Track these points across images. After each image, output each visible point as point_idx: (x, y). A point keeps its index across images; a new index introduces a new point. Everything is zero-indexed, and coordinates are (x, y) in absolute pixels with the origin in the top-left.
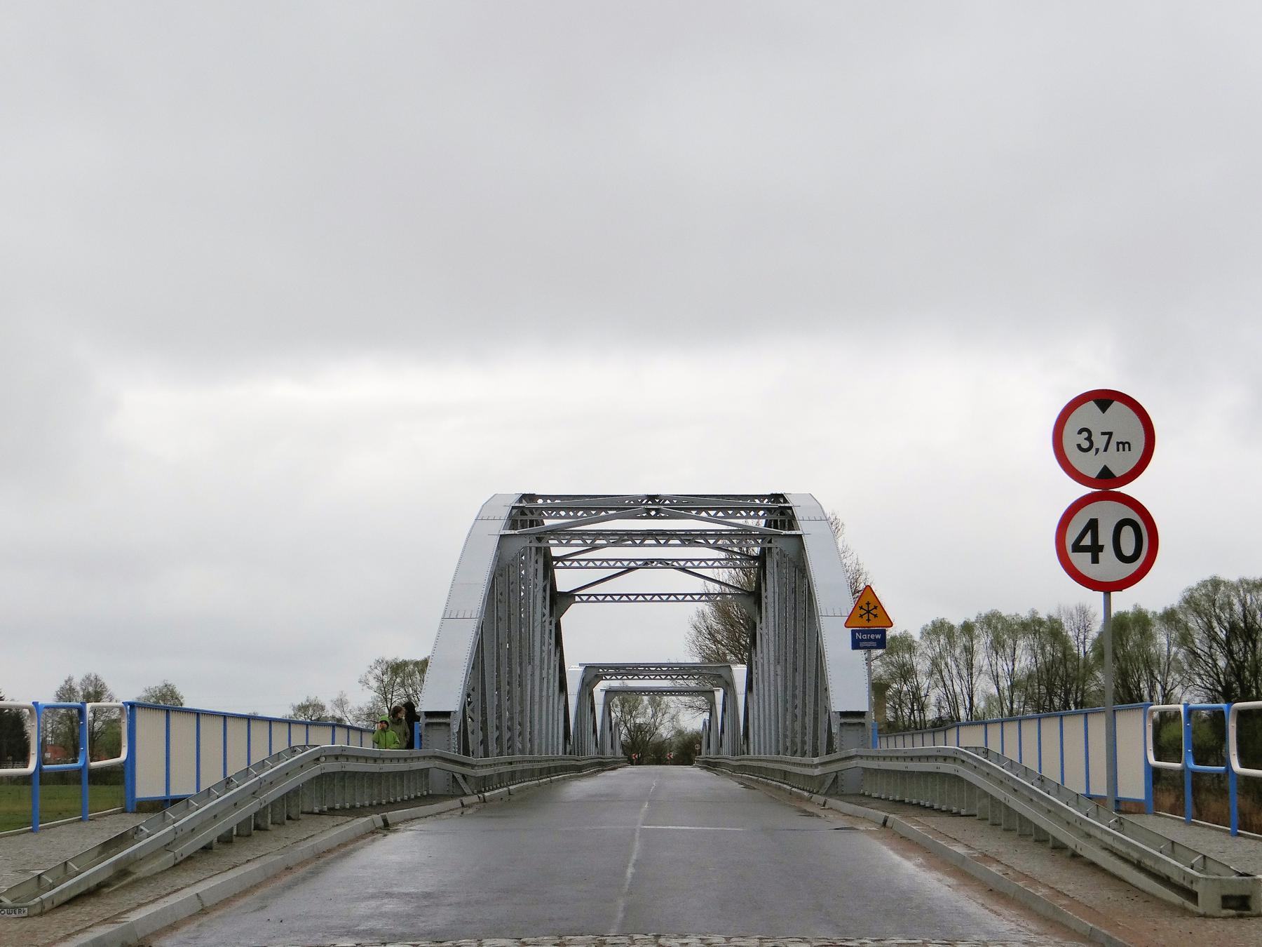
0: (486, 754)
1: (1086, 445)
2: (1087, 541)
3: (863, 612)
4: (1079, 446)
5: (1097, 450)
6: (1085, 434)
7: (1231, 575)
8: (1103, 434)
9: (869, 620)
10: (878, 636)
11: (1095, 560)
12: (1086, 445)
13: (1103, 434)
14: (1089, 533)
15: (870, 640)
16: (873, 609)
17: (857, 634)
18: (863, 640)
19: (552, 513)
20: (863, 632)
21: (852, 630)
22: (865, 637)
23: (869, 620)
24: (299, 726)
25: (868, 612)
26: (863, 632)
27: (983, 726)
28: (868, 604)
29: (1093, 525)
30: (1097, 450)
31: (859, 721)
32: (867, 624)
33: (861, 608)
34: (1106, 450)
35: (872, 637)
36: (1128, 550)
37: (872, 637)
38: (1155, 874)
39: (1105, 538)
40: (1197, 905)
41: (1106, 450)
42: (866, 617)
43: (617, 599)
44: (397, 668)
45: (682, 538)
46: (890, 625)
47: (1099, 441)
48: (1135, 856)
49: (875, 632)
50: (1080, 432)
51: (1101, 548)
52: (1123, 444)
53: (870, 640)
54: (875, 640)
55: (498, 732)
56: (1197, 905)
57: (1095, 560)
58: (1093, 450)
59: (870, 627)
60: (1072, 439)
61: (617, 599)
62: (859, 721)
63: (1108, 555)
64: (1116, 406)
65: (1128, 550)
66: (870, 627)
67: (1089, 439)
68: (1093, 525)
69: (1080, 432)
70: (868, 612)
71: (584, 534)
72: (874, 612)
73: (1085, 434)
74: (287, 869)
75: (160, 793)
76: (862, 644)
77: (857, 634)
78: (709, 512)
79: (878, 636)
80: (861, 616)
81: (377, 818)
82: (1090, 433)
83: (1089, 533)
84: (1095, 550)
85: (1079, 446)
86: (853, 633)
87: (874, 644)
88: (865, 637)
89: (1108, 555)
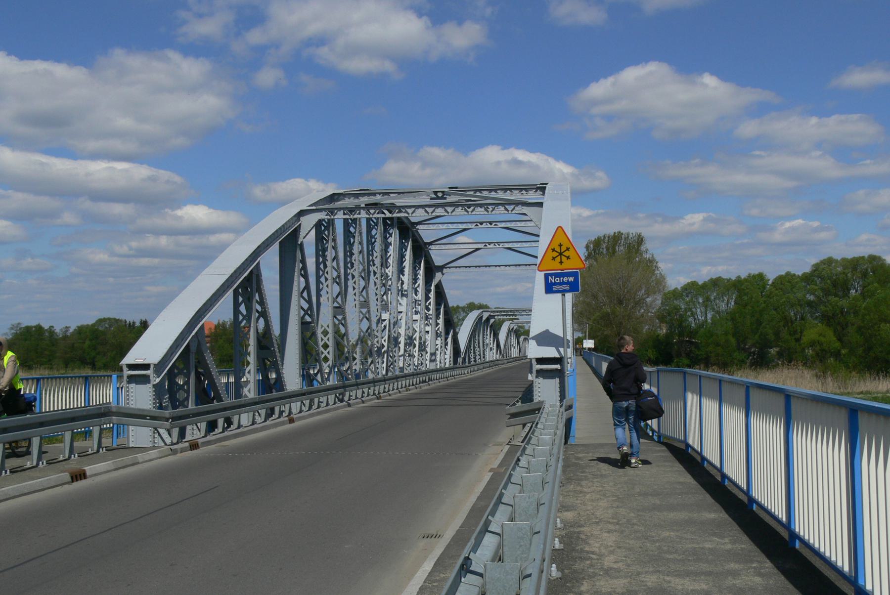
3: (564, 248)
9: (561, 262)
10: (571, 279)
14: (306, 290)
15: (560, 284)
17: (550, 278)
18: (556, 284)
19: (324, 225)
21: (545, 274)
22: (558, 280)
23: (561, 262)
24: (103, 471)
26: (556, 275)
28: (560, 245)
32: (560, 266)
33: (568, 249)
35: (565, 279)
37: (565, 279)
40: (440, 281)
42: (558, 259)
43: (440, 196)
46: (540, 269)
49: (568, 275)
53: (560, 284)
54: (568, 283)
56: (440, 281)
61: (440, 196)
70: (561, 254)
71: (446, 206)
76: (555, 288)
79: (571, 279)
83: (306, 290)
86: (546, 276)
87: (567, 287)
88: (558, 280)
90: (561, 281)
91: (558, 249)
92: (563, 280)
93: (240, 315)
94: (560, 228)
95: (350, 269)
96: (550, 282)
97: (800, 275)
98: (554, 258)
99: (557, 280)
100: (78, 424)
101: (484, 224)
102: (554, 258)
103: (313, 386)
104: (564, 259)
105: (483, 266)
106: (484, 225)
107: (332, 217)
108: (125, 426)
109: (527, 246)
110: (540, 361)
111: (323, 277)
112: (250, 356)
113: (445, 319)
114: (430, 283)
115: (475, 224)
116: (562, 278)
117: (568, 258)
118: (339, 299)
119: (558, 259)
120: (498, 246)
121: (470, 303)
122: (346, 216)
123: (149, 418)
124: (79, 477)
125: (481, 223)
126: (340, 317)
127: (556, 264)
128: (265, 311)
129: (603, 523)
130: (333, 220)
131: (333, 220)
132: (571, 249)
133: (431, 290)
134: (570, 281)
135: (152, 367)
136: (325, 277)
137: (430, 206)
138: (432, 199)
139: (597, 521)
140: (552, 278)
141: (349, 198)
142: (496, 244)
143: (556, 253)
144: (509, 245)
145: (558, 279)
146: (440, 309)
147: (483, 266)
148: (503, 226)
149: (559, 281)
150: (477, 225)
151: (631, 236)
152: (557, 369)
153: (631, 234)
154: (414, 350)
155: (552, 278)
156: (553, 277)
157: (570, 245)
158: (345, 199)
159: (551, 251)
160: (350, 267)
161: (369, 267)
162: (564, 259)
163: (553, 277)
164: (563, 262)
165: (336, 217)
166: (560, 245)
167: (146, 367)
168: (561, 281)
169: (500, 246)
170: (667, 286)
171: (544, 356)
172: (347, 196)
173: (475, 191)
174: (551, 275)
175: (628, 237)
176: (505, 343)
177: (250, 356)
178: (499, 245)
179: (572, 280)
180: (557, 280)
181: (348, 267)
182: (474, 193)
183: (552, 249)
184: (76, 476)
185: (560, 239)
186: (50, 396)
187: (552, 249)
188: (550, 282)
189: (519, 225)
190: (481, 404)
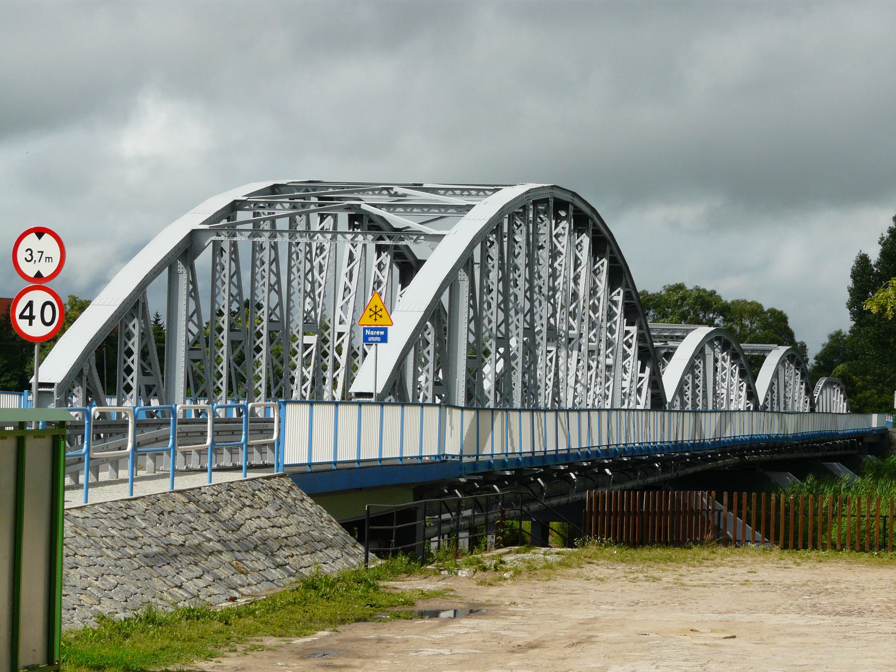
0: (250, 422)
1: (29, 258)
2: (27, 313)
4: (26, 259)
5: (35, 261)
6: (29, 252)
7: (850, 274)
8: (39, 252)
9: (381, 310)
10: (382, 333)
11: (31, 324)
12: (29, 258)
13: (39, 252)
14: (29, 308)
15: (375, 336)
18: (371, 336)
22: (372, 333)
23: (371, 310)
27: (587, 413)
29: (30, 304)
30: (35, 261)
31: (50, 390)
34: (39, 261)
35: (378, 333)
36: (48, 319)
38: (396, 484)
39: (37, 312)
41: (39, 261)
42: (374, 317)
47: (36, 256)
50: (27, 251)
51: (34, 317)
52: (49, 258)
53: (375, 336)
54: (379, 336)
57: (31, 324)
58: (33, 261)
59: (377, 325)
60: (22, 254)
62: (50, 390)
63: (37, 321)
64: (46, 236)
65: (48, 319)
66: (377, 325)
67: (31, 255)
68: (30, 304)
69: (27, 251)
73: (29, 252)
74: (722, 630)
79: (382, 333)
80: (370, 316)
83: (29, 308)
84: (31, 318)
85: (26, 259)
86: (365, 329)
87: (379, 339)
88: (372, 333)
89: (37, 321)
93: (529, 297)
95: (259, 269)
103: (626, 326)
104: (378, 317)
108: (592, 413)
111: (295, 267)
113: (640, 348)
118: (502, 328)
119: (374, 317)
126: (501, 350)
128: (726, 310)
129: (270, 560)
135: (56, 386)
136: (297, 267)
139: (685, 302)
154: (304, 387)
160: (259, 265)
161: (533, 295)
162: (378, 317)
167: (51, 385)
174: (368, 329)
176: (772, 384)
181: (256, 265)
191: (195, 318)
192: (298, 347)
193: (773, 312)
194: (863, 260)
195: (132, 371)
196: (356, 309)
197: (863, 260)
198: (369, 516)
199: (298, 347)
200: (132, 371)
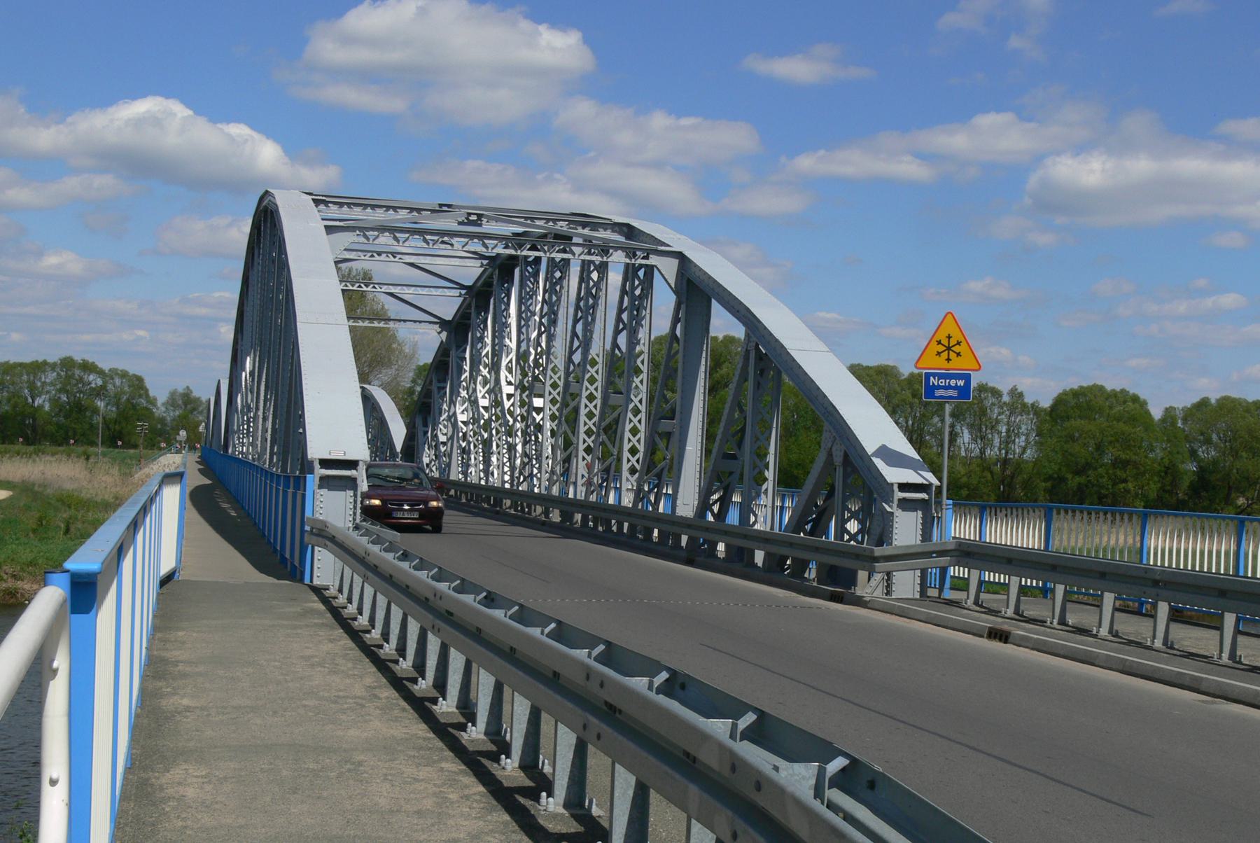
3: (953, 342)
9: (948, 360)
10: (961, 383)
15: (945, 388)
16: (943, 345)
17: (932, 378)
18: (939, 387)
20: (941, 376)
22: (942, 383)
23: (948, 360)
25: (949, 348)
26: (941, 376)
28: (949, 337)
35: (953, 383)
37: (953, 383)
42: (945, 355)
44: (842, 598)
45: (428, 237)
46: (978, 367)
48: (361, 553)
53: (945, 388)
54: (956, 387)
55: (375, 322)
72: (957, 349)
75: (916, 571)
77: (932, 378)
78: (521, 339)
79: (961, 383)
81: (490, 475)
82: (951, 313)
88: (942, 383)
90: (947, 384)
91: (945, 342)
92: (949, 382)
94: (950, 315)
96: (931, 384)
97: (1213, 401)
98: (939, 354)
99: (942, 382)
100: (905, 564)
101: (384, 255)
102: (939, 354)
104: (952, 355)
105: (411, 321)
106: (383, 257)
107: (605, 259)
109: (438, 293)
110: (904, 487)
112: (768, 470)
114: (463, 348)
115: (370, 254)
116: (948, 381)
117: (958, 354)
119: (945, 355)
120: (379, 290)
121: (65, 359)
122: (540, 253)
123: (935, 555)
124: (993, 635)
125: (379, 254)
127: (941, 362)
130: (607, 263)
131: (607, 263)
132: (937, 338)
133: (465, 358)
134: (959, 385)
137: (402, 230)
138: (460, 223)
140: (935, 379)
141: (605, 230)
142: (376, 286)
143: (954, 344)
144: (392, 290)
145: (943, 381)
146: (446, 387)
147: (411, 321)
148: (412, 261)
149: (943, 384)
150: (372, 256)
151: (354, 273)
152: (923, 500)
153: (354, 271)
155: (935, 379)
156: (936, 378)
157: (963, 338)
158: (598, 231)
159: (934, 343)
162: (952, 355)
163: (936, 378)
164: (951, 360)
165: (609, 260)
166: (949, 337)
168: (947, 384)
169: (383, 290)
170: (416, 356)
171: (909, 482)
172: (603, 226)
173: (548, 220)
174: (934, 375)
175: (349, 274)
177: (768, 470)
178: (381, 288)
179: (962, 385)
180: (942, 382)
182: (545, 223)
183: (961, 342)
184: (996, 634)
185: (949, 328)
186: (965, 528)
187: (961, 342)
188: (931, 384)
189: (423, 261)
190: (486, 533)
191: (621, 326)
192: (628, 459)
193: (135, 376)
194: (199, 470)
195: (630, 431)
196: (1120, 668)
197: (199, 470)
198: (916, 600)
199: (628, 459)
200: (630, 431)
